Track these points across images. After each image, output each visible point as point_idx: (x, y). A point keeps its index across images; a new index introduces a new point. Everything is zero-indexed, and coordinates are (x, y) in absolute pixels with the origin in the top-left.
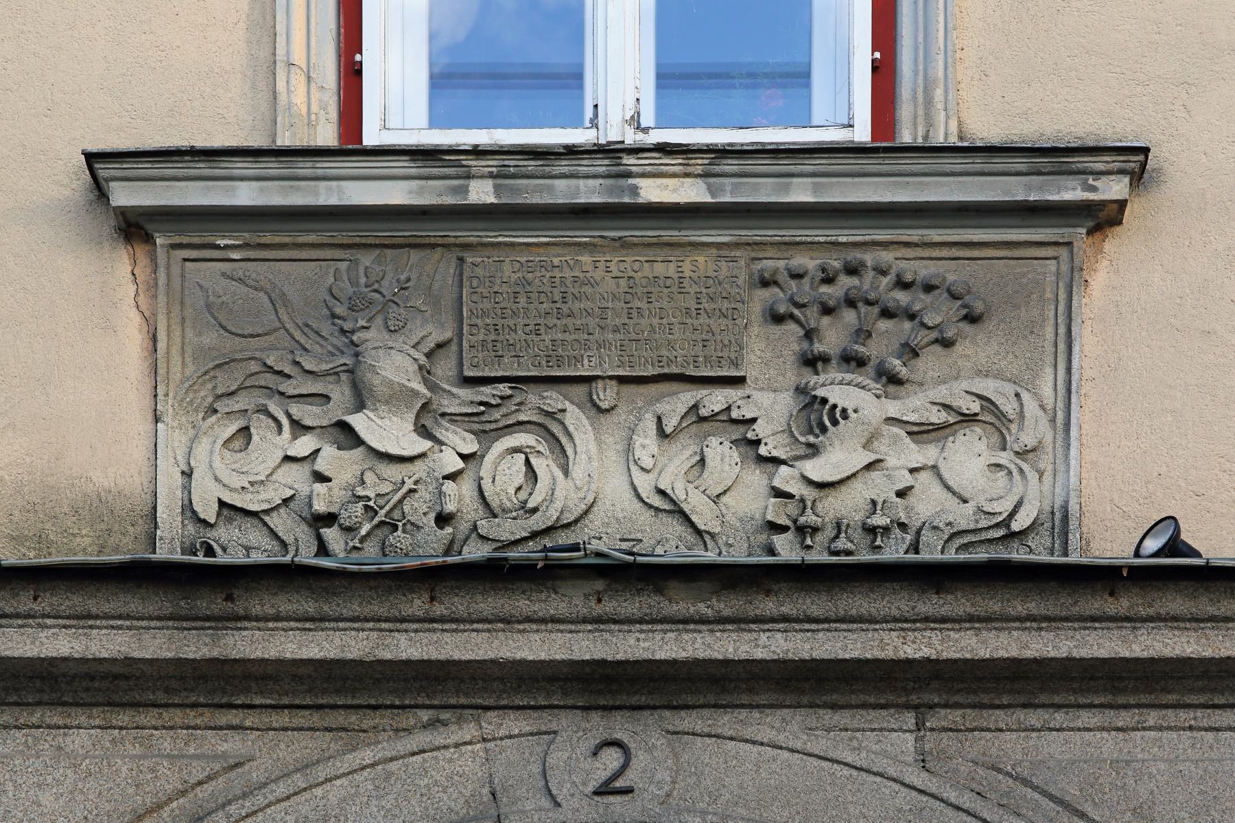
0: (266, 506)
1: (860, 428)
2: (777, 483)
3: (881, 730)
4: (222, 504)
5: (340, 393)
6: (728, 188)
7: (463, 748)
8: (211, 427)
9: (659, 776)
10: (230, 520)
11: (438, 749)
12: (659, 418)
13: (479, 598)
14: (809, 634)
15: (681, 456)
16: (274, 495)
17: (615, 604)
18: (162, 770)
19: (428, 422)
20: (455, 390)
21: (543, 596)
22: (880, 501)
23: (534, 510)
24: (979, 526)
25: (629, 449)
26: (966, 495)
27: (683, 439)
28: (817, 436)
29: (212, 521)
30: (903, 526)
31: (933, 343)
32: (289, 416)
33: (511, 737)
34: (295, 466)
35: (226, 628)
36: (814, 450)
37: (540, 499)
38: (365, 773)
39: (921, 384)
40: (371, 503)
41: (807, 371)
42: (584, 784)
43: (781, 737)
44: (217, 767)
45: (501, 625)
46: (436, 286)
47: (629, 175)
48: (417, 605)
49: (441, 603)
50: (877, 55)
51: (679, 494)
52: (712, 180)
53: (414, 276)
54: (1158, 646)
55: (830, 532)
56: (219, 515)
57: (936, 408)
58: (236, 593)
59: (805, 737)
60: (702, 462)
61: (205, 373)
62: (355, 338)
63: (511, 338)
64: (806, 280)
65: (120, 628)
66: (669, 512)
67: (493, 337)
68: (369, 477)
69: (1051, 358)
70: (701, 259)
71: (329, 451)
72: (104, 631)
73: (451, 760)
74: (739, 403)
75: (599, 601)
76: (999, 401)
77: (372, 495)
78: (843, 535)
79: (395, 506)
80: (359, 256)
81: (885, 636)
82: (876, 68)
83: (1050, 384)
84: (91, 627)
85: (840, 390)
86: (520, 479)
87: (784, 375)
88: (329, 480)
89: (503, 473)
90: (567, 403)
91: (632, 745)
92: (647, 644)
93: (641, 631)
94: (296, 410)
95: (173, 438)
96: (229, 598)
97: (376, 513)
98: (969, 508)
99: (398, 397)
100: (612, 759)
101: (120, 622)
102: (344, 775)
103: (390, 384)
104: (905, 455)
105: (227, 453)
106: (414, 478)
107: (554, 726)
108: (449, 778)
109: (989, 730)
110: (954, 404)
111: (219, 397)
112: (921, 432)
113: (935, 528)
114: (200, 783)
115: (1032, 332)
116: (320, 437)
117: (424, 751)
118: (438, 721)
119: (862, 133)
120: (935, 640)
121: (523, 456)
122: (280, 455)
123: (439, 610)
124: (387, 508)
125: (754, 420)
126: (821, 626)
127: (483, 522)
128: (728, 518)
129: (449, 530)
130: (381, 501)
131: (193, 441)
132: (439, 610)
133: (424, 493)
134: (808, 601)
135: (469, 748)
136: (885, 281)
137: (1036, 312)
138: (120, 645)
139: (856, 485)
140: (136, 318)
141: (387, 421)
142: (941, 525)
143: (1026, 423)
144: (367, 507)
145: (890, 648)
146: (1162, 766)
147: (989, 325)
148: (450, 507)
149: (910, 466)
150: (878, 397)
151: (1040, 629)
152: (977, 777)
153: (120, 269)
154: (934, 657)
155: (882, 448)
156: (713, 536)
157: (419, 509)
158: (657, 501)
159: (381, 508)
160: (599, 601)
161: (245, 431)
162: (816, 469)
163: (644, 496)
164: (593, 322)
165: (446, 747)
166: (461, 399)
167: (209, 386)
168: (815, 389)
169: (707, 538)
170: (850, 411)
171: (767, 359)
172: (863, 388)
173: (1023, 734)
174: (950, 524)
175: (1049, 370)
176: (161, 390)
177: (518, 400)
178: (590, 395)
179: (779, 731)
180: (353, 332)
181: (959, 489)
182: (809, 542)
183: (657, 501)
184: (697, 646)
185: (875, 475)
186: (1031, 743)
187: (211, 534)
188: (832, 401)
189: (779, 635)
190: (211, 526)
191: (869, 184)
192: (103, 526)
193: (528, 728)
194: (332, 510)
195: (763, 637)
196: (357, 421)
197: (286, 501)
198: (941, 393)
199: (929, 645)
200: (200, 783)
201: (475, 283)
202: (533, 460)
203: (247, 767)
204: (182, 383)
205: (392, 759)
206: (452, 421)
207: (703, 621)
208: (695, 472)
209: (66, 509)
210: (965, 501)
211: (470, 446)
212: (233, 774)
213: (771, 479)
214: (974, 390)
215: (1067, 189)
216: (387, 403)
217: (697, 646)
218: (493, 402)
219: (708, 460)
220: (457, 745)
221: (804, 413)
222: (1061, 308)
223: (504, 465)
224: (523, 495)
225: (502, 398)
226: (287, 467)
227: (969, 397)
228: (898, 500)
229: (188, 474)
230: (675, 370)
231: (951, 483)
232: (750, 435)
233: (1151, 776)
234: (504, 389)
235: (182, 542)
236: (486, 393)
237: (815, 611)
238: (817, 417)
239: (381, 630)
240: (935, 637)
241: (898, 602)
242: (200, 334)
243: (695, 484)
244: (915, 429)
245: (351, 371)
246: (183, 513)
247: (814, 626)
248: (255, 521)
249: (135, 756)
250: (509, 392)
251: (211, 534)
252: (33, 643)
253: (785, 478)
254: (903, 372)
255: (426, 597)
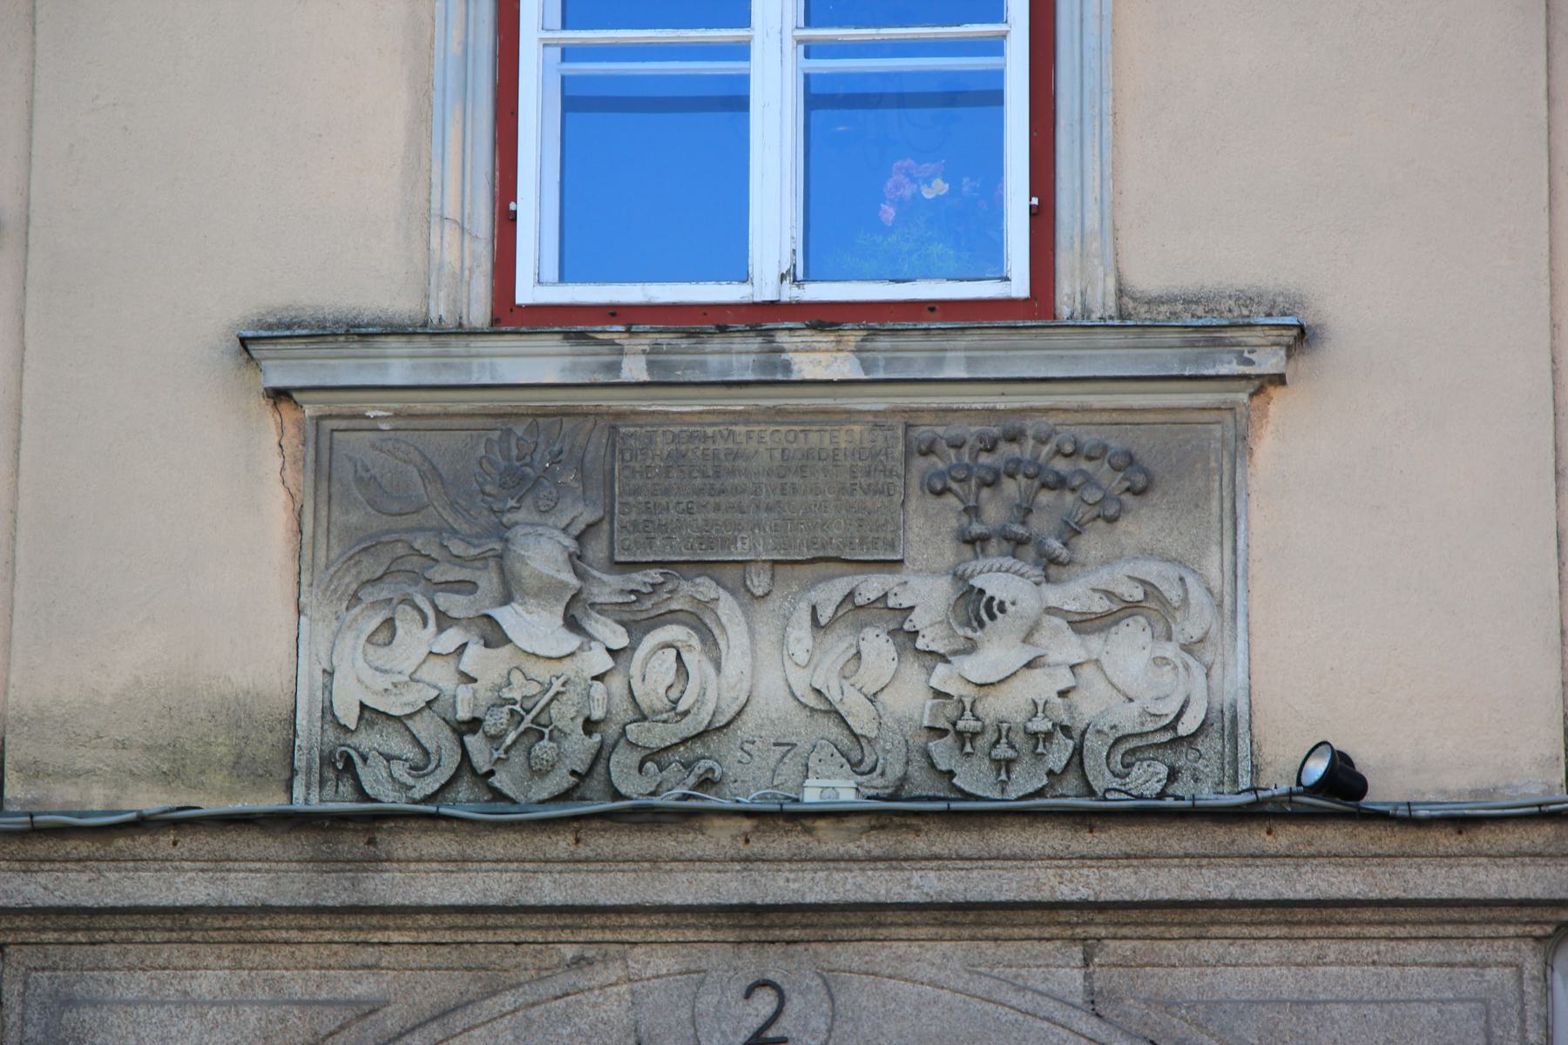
0: (408, 710)
1: (1018, 622)
2: (934, 682)
3: (1047, 966)
4: (363, 706)
5: (488, 581)
6: (882, 363)
7: (608, 990)
8: (355, 620)
9: (813, 1024)
10: (371, 724)
11: (582, 991)
12: (814, 608)
13: (625, 839)
14: (963, 873)
15: (839, 646)
16: (418, 696)
17: (762, 844)
18: (292, 1020)
19: (578, 612)
20: (605, 577)
21: (690, 837)
22: (1041, 704)
23: (686, 713)
24: (1146, 729)
25: (783, 642)
26: (1131, 695)
27: (839, 629)
28: (975, 631)
29: (353, 727)
30: (1066, 730)
31: (1094, 519)
32: (435, 607)
33: (658, 977)
34: (439, 661)
35: (366, 870)
36: (971, 648)
37: (691, 701)
38: (505, 1021)
39: (1084, 565)
40: (517, 707)
41: (967, 551)
42: (735, 1033)
43: (942, 975)
44: (349, 1014)
45: (646, 865)
46: (589, 457)
47: (782, 351)
48: (562, 844)
49: (587, 845)
50: (1035, 201)
51: (834, 695)
52: (864, 355)
53: (566, 448)
54: (1323, 886)
55: (991, 736)
56: (360, 718)
57: (1097, 595)
58: (379, 836)
59: (967, 976)
60: (858, 655)
61: (351, 558)
62: (505, 520)
63: (664, 518)
64: (966, 450)
65: (258, 871)
66: (825, 712)
67: (645, 517)
68: (517, 678)
69: (1217, 535)
70: (857, 428)
71: (475, 651)
72: (241, 875)
73: (595, 1005)
74: (896, 590)
75: (747, 841)
76: (1164, 587)
77: (518, 698)
78: (1004, 740)
79: (542, 710)
80: (510, 426)
81: (1041, 873)
82: (1034, 213)
83: (1217, 563)
84: (229, 870)
85: (1000, 579)
86: (670, 677)
87: (942, 555)
88: (475, 680)
89: (653, 673)
90: (721, 591)
91: (785, 987)
92: (796, 885)
93: (791, 871)
94: (442, 600)
95: (317, 631)
96: (371, 842)
97: (523, 718)
98: (1135, 708)
99: (546, 590)
100: (765, 1003)
101: (258, 865)
102: (484, 1023)
103: (540, 576)
104: (1066, 647)
105: (371, 649)
106: (562, 680)
107: (703, 964)
108: (593, 1026)
109: (1160, 965)
110: (1116, 591)
111: (364, 584)
112: (1082, 624)
113: (1099, 732)
114: (331, 1034)
115: (1197, 506)
116: (467, 629)
117: (568, 994)
118: (583, 958)
119: (1019, 286)
120: (1093, 880)
121: (674, 652)
122: (426, 651)
123: (583, 851)
124: (534, 713)
125: (912, 608)
126: (975, 864)
127: (633, 726)
128: (885, 719)
129: (597, 738)
130: (528, 705)
131: (336, 634)
132: (583, 851)
133: (572, 696)
134: (960, 841)
135: (615, 989)
136: (1046, 450)
137: (1200, 484)
138: (258, 891)
139: (1016, 683)
140: (281, 496)
141: (535, 617)
142: (1106, 729)
143: (1192, 611)
144: (512, 712)
145: (1046, 888)
146: (1345, 1009)
147: (1154, 497)
148: (597, 714)
149: (1075, 663)
150: (1037, 584)
151: (1201, 867)
152: (1150, 1022)
153: (268, 425)
154: (1092, 899)
155: (1042, 638)
156: (869, 741)
157: (565, 714)
158: (812, 701)
159: (528, 712)
160: (747, 841)
161: (389, 623)
162: (976, 667)
163: (798, 694)
164: (746, 499)
165: (590, 989)
166: (609, 586)
167: (354, 571)
168: (972, 576)
169: (864, 742)
170: (1007, 605)
171: (928, 532)
172: (1022, 575)
173: (1197, 970)
174: (1114, 727)
175: (1215, 549)
176: (305, 579)
177: (670, 586)
178: (744, 579)
179: (939, 969)
180: (502, 512)
181: (1128, 680)
182: (968, 749)
183: (812, 701)
184: (848, 887)
185: (1037, 673)
186: (1207, 980)
187: (353, 740)
188: (989, 593)
189: (932, 874)
190: (352, 732)
191: (1023, 358)
192: (241, 733)
193: (676, 967)
194: (477, 715)
195: (916, 876)
196: (506, 617)
197: (429, 704)
198: (1103, 578)
199: (1087, 885)
200: (331, 1034)
201: (627, 456)
202: (685, 656)
203: (381, 1014)
204: (327, 568)
205: (533, 1005)
206: (600, 612)
207: (853, 859)
208: (852, 666)
209: (203, 714)
210: (1131, 700)
211: (620, 640)
212: (366, 1023)
213: (927, 681)
214: (1137, 575)
215: (1222, 362)
216: (536, 596)
217: (848, 887)
218: (644, 590)
219: (864, 655)
220: (601, 988)
221: (961, 602)
222: (1226, 480)
223: (654, 662)
224: (674, 694)
225: (653, 585)
226: (433, 659)
227: (1131, 584)
228: (1059, 700)
229: (329, 674)
230: (832, 553)
231: (1115, 680)
232: (907, 627)
233: (1333, 1021)
234: (655, 575)
235: (321, 751)
236: (638, 579)
237: (966, 850)
238: (976, 609)
239: (525, 871)
240: (1092, 875)
241: (1051, 838)
242: (347, 512)
243: (852, 681)
244: (1077, 618)
245: (500, 557)
246: (323, 717)
247: (967, 864)
248: (398, 725)
249: (263, 1002)
250: (661, 579)
251: (353, 740)
252: (168, 889)
253: (941, 676)
254: (1064, 554)
255: (571, 839)
